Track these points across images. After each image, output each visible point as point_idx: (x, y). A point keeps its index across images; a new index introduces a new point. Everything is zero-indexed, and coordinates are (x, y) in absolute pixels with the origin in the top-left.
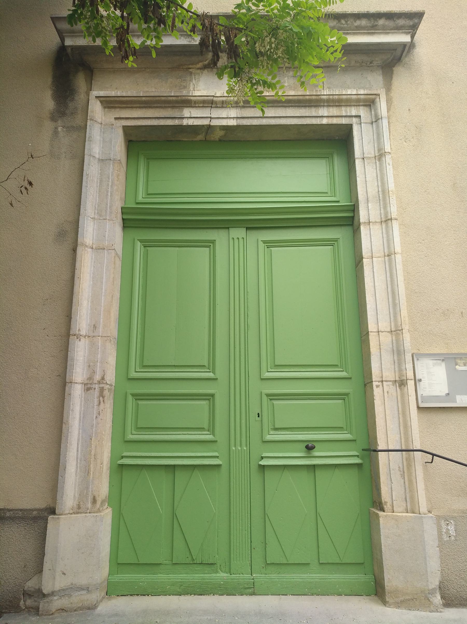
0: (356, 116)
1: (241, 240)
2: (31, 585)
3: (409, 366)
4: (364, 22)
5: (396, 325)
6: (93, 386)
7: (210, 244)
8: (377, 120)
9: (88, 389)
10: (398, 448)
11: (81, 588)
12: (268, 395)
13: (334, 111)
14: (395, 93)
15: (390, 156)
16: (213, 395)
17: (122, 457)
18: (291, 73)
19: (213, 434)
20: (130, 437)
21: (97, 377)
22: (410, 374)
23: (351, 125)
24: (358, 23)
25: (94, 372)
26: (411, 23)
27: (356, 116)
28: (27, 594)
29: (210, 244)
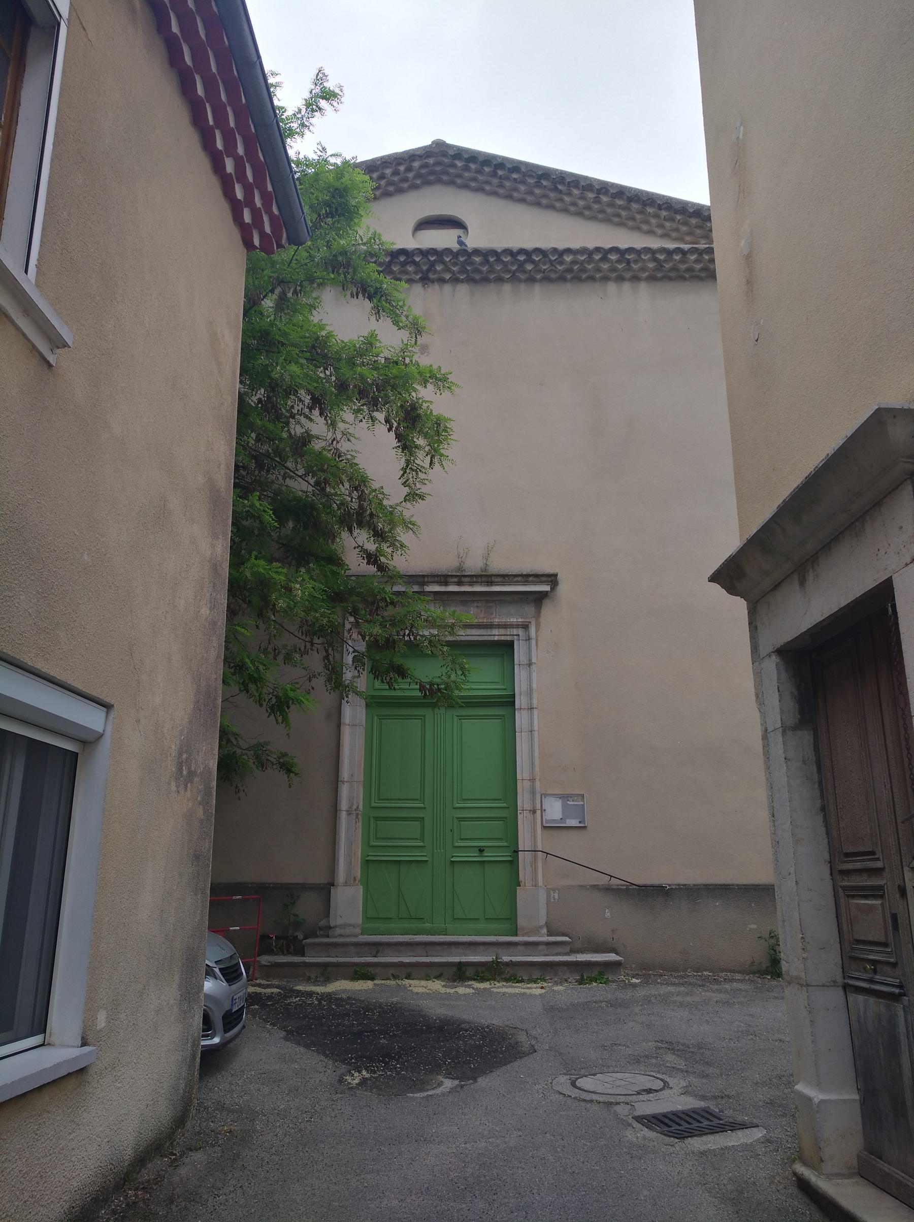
0: (516, 635)
1: (442, 715)
2: (323, 923)
3: (538, 802)
4: (520, 579)
5: (533, 777)
6: (352, 812)
7: (422, 816)
8: (529, 639)
9: (349, 814)
10: (530, 850)
11: (350, 925)
12: (457, 818)
13: (502, 631)
14: (542, 620)
15: (535, 665)
16: (423, 818)
17: (368, 856)
18: (475, 604)
19: (423, 842)
20: (372, 844)
21: (355, 807)
22: (538, 806)
23: (513, 641)
24: (516, 579)
25: (353, 804)
26: (550, 579)
27: (516, 635)
28: (321, 929)
29: (423, 718)
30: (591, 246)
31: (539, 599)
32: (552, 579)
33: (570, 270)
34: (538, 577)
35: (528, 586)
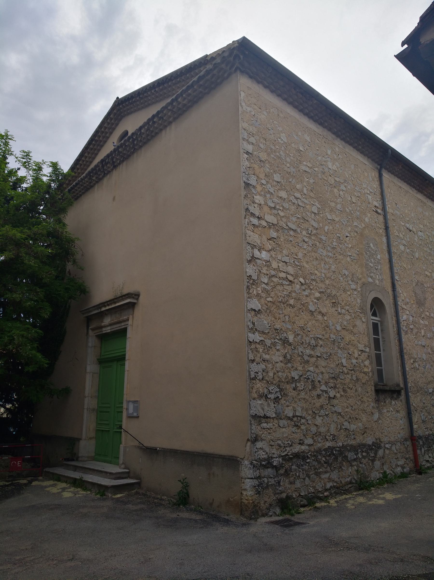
30: (146, 120)
31: (132, 306)
32: (137, 296)
33: (148, 135)
34: (128, 295)
35: (125, 301)
